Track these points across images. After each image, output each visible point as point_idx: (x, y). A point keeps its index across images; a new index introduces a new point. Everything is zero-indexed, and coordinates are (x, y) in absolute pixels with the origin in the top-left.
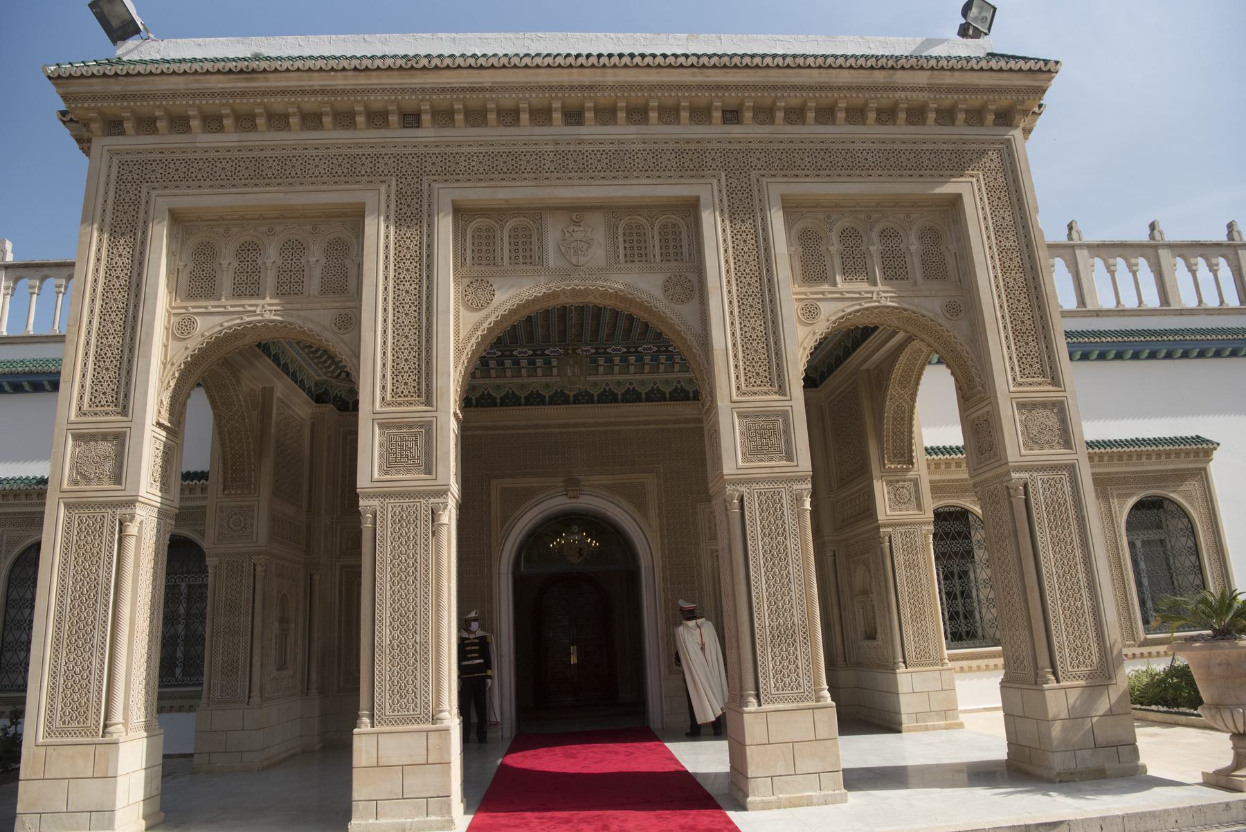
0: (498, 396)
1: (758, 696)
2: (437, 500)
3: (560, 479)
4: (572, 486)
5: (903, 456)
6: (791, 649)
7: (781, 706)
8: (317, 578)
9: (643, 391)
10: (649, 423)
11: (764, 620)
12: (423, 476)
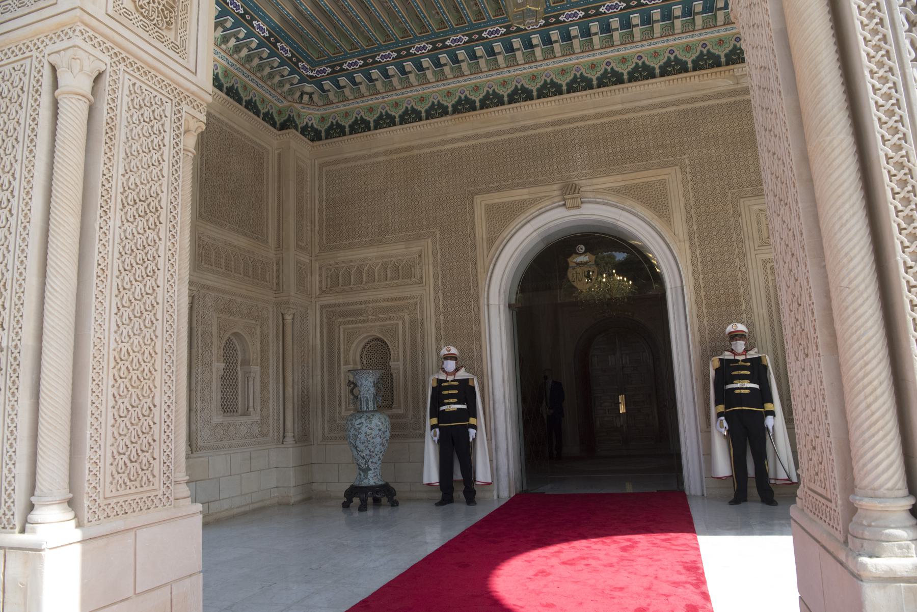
0: (477, 98)
3: (556, 187)
4: (571, 193)
8: (289, 318)
10: (602, 115)
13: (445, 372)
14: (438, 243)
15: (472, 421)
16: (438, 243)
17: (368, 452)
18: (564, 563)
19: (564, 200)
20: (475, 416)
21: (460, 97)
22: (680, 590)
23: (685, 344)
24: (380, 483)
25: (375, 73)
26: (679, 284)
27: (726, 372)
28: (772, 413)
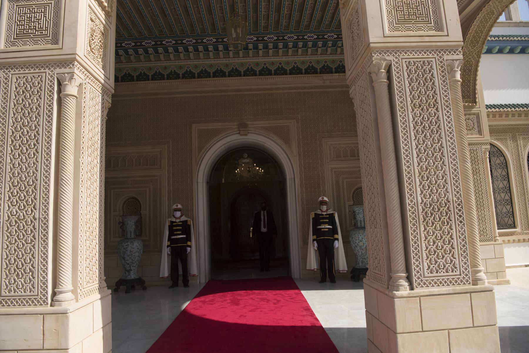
1: (409, 279)
2: (63, 70)
3: (235, 123)
5: (469, 97)
6: (446, 228)
7: (435, 290)
9: (288, 68)
11: (416, 196)
12: (50, 46)
13: (175, 217)
14: (171, 147)
15: (189, 243)
16: (171, 147)
17: (131, 261)
18: (250, 311)
19: (239, 131)
20: (190, 241)
21: (187, 70)
22: (306, 318)
23: (294, 206)
24: (137, 277)
25: (141, 51)
26: (293, 177)
27: (318, 220)
28: (337, 239)
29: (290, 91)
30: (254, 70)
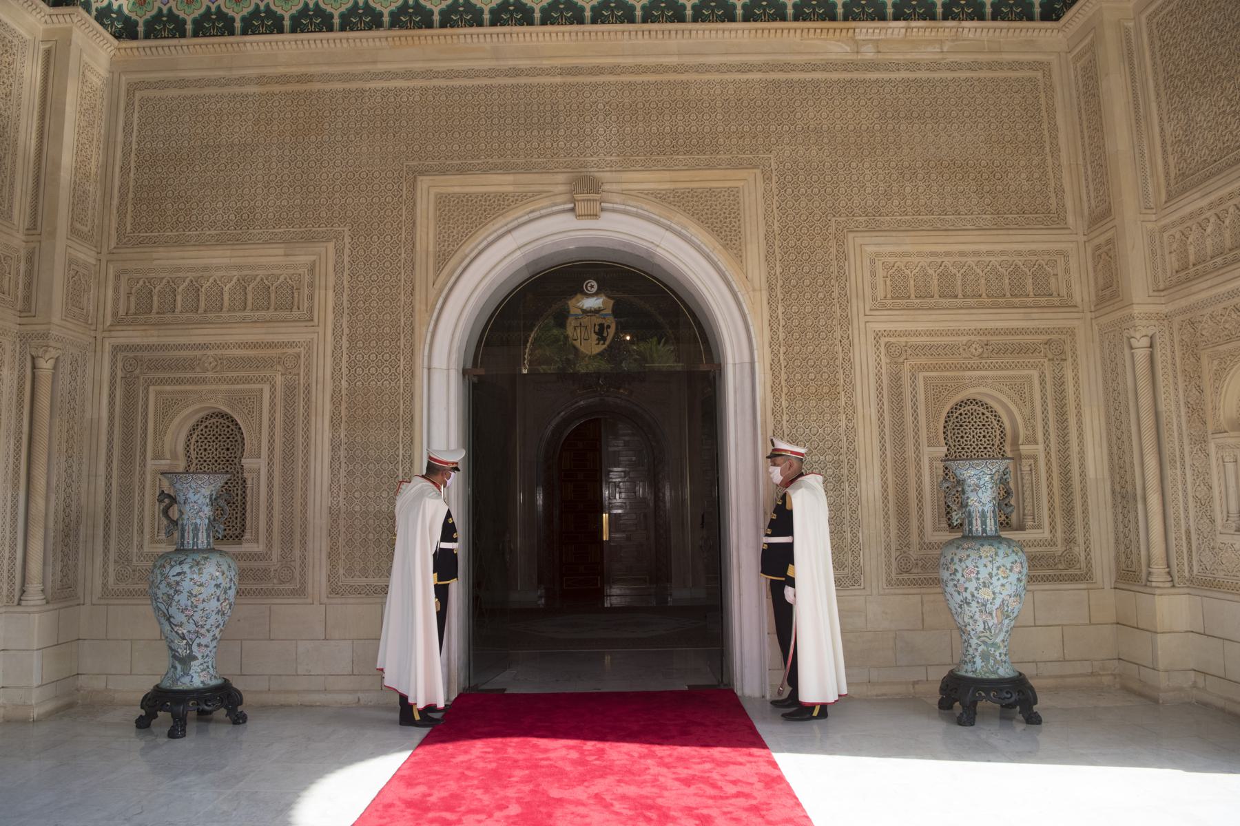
3: (561, 178)
14: (347, 251)
16: (347, 251)
17: (192, 627)
19: (574, 201)
24: (214, 682)
26: (747, 359)
29: (745, 77)
30: (374, 10)
